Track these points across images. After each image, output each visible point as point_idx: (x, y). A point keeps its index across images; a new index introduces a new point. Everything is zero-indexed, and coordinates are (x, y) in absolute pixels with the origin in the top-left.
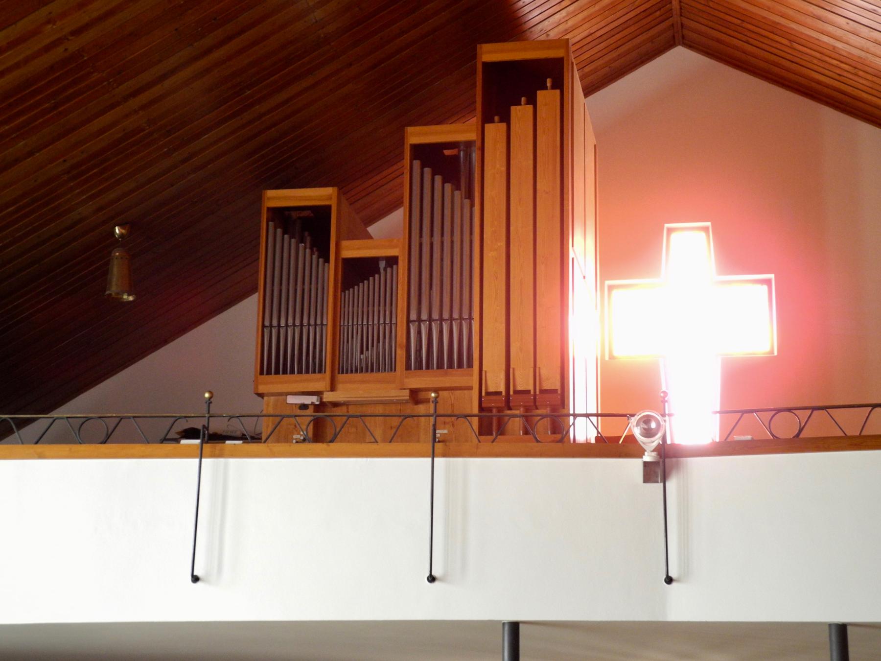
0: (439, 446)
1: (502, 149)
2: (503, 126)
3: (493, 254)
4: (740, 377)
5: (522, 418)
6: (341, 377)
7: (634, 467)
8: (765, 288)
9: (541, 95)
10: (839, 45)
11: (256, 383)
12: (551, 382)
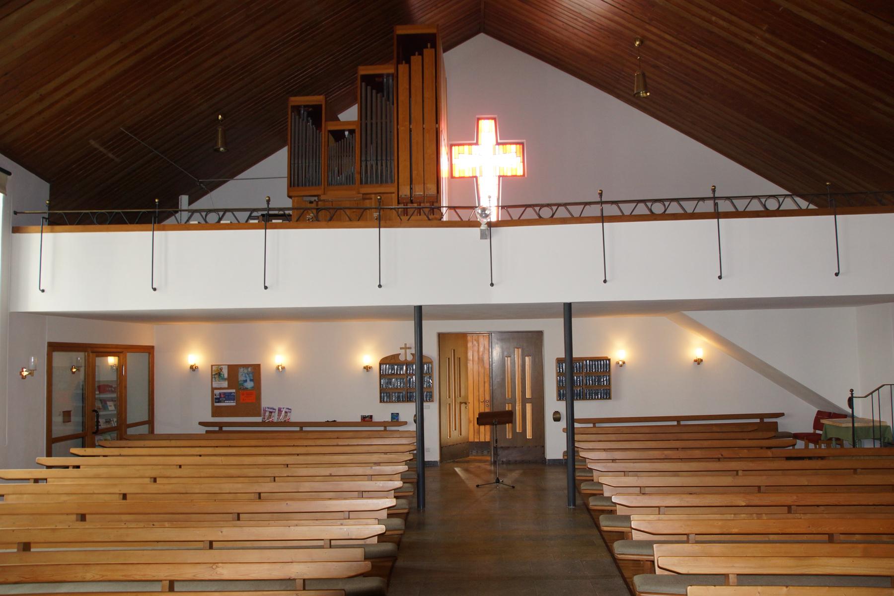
0: (381, 222)
1: (406, 77)
5: (423, 209)
7: (476, 231)
9: (425, 50)
10: (558, 35)
11: (466, 218)
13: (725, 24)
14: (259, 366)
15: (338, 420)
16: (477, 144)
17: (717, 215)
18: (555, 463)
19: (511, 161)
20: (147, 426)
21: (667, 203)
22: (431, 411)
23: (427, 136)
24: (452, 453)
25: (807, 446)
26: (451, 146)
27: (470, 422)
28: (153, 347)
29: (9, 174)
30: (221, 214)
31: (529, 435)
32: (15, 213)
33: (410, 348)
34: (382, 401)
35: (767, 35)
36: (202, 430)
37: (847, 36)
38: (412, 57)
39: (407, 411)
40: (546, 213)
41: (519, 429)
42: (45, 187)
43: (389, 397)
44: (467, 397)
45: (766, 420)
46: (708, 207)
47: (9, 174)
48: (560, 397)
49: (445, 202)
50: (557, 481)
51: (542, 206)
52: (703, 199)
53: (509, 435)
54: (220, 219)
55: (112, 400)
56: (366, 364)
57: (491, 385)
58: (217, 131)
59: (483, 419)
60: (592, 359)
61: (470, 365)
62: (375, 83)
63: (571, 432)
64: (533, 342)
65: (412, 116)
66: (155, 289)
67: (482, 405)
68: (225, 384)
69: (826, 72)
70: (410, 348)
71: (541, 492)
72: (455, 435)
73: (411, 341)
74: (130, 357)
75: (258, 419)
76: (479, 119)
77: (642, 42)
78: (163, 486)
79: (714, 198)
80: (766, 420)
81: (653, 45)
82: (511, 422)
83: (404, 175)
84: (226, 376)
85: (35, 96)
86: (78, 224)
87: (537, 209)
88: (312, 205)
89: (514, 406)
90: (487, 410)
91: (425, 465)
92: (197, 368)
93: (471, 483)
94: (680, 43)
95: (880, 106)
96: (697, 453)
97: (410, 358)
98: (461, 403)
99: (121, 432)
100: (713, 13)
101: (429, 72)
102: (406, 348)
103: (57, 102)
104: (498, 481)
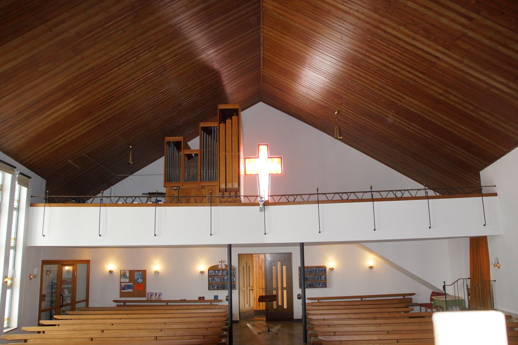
0: (212, 202)
1: (224, 130)
4: (274, 178)
5: (231, 197)
7: (257, 208)
8: (279, 159)
13: (376, 109)
14: (145, 271)
15: (187, 299)
16: (258, 158)
17: (373, 200)
18: (298, 321)
19: (276, 166)
20: (85, 302)
21: (349, 194)
22: (235, 293)
23: (234, 159)
24: (245, 316)
25: (426, 310)
26: (245, 159)
27: (255, 299)
28: (89, 261)
29: (30, 178)
30: (133, 198)
31: (285, 307)
32: (32, 197)
33: (224, 262)
34: (209, 289)
35: (395, 115)
36: (115, 305)
37: (428, 118)
38: (227, 120)
39: (223, 294)
40: (291, 199)
41: (280, 304)
42: (44, 181)
43: (213, 287)
44: (253, 286)
45: (406, 297)
46: (368, 196)
47: (30, 178)
48: (300, 286)
49: (242, 193)
50: (299, 330)
51: (289, 195)
52: (366, 192)
53: (275, 307)
54: (133, 201)
55: (67, 288)
56: (201, 270)
57: (266, 281)
58: (129, 154)
59: (261, 299)
60: (317, 267)
61: (255, 270)
62: (208, 131)
63: (304, 304)
64: (287, 259)
66: (100, 236)
67: (261, 291)
68: (127, 280)
69: (422, 131)
70: (224, 262)
71: (291, 336)
72: (247, 306)
73: (226, 258)
74: (79, 266)
75: (145, 299)
76: (259, 145)
77: (338, 112)
78: (106, 334)
79: (372, 192)
80: (406, 297)
81: (343, 114)
82: (275, 300)
83: (222, 178)
84: (128, 276)
85: (48, 143)
87: (287, 197)
88: (177, 192)
89: (277, 292)
90: (264, 294)
91: (233, 322)
92: (112, 272)
93: (255, 331)
94: (356, 114)
95: (448, 147)
96: (364, 316)
97: (224, 267)
98: (250, 290)
99: (73, 307)
100: (369, 103)
101: (235, 127)
102: (222, 262)
103: (57, 145)
104: (269, 331)
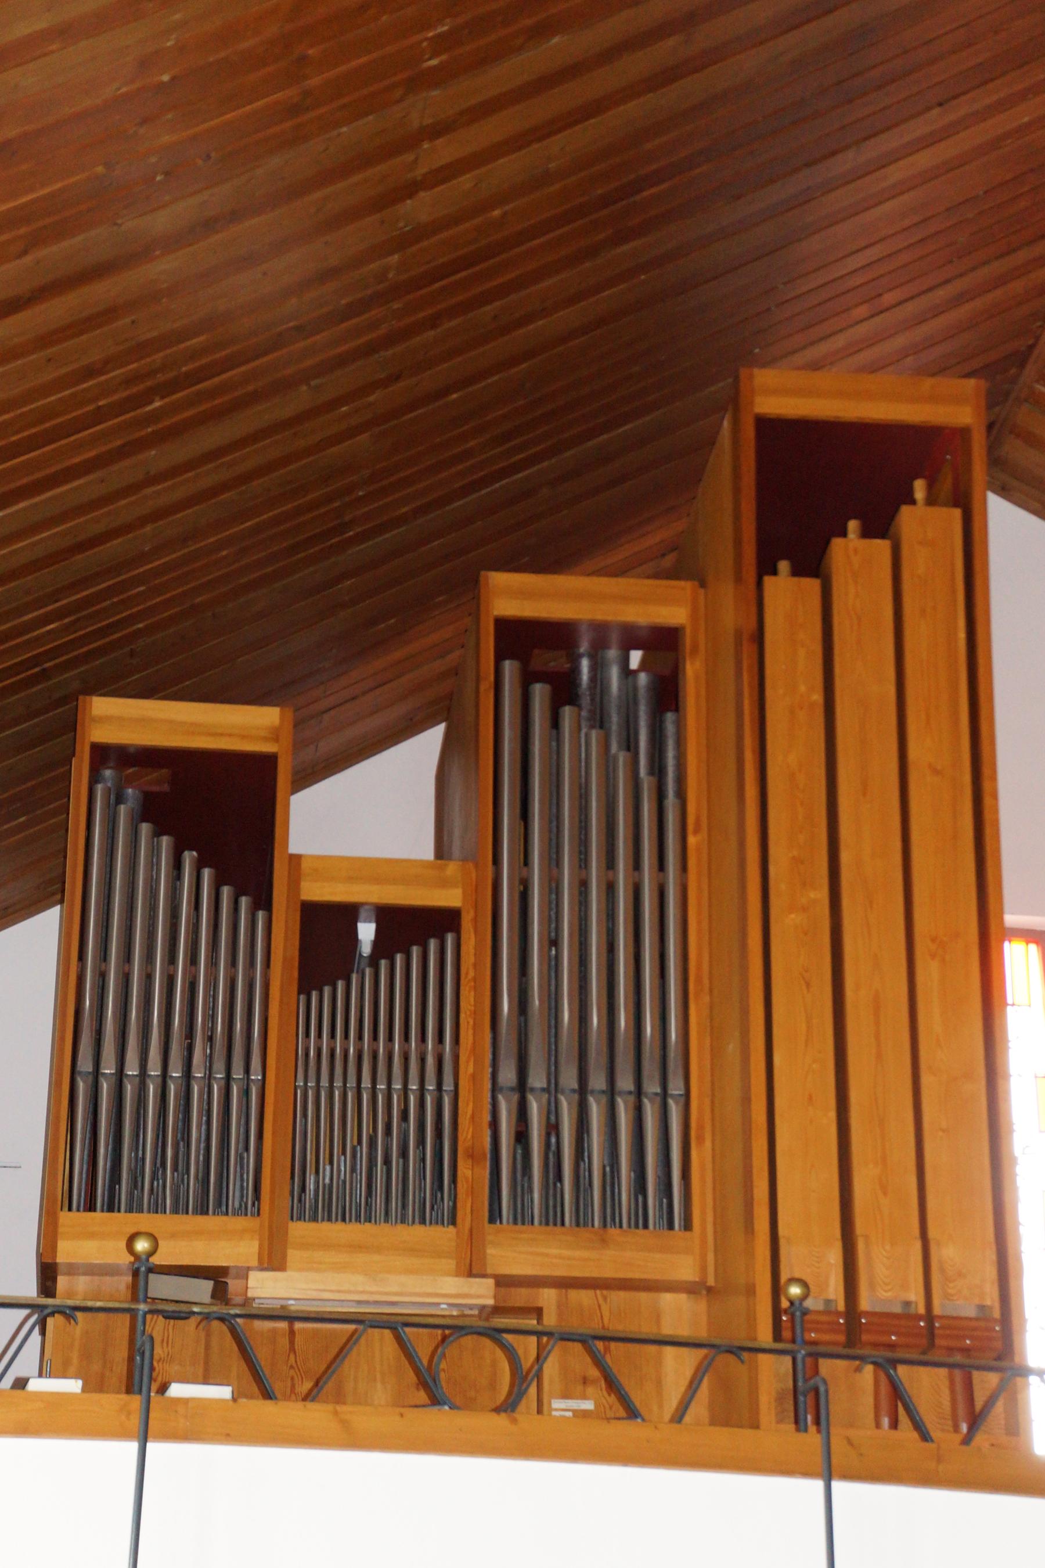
2: (812, 585)
3: (794, 919)
6: (299, 1230)
7: (193, 1321)
12: (963, 1297)
65: (846, 857)
86: (533, 572)
